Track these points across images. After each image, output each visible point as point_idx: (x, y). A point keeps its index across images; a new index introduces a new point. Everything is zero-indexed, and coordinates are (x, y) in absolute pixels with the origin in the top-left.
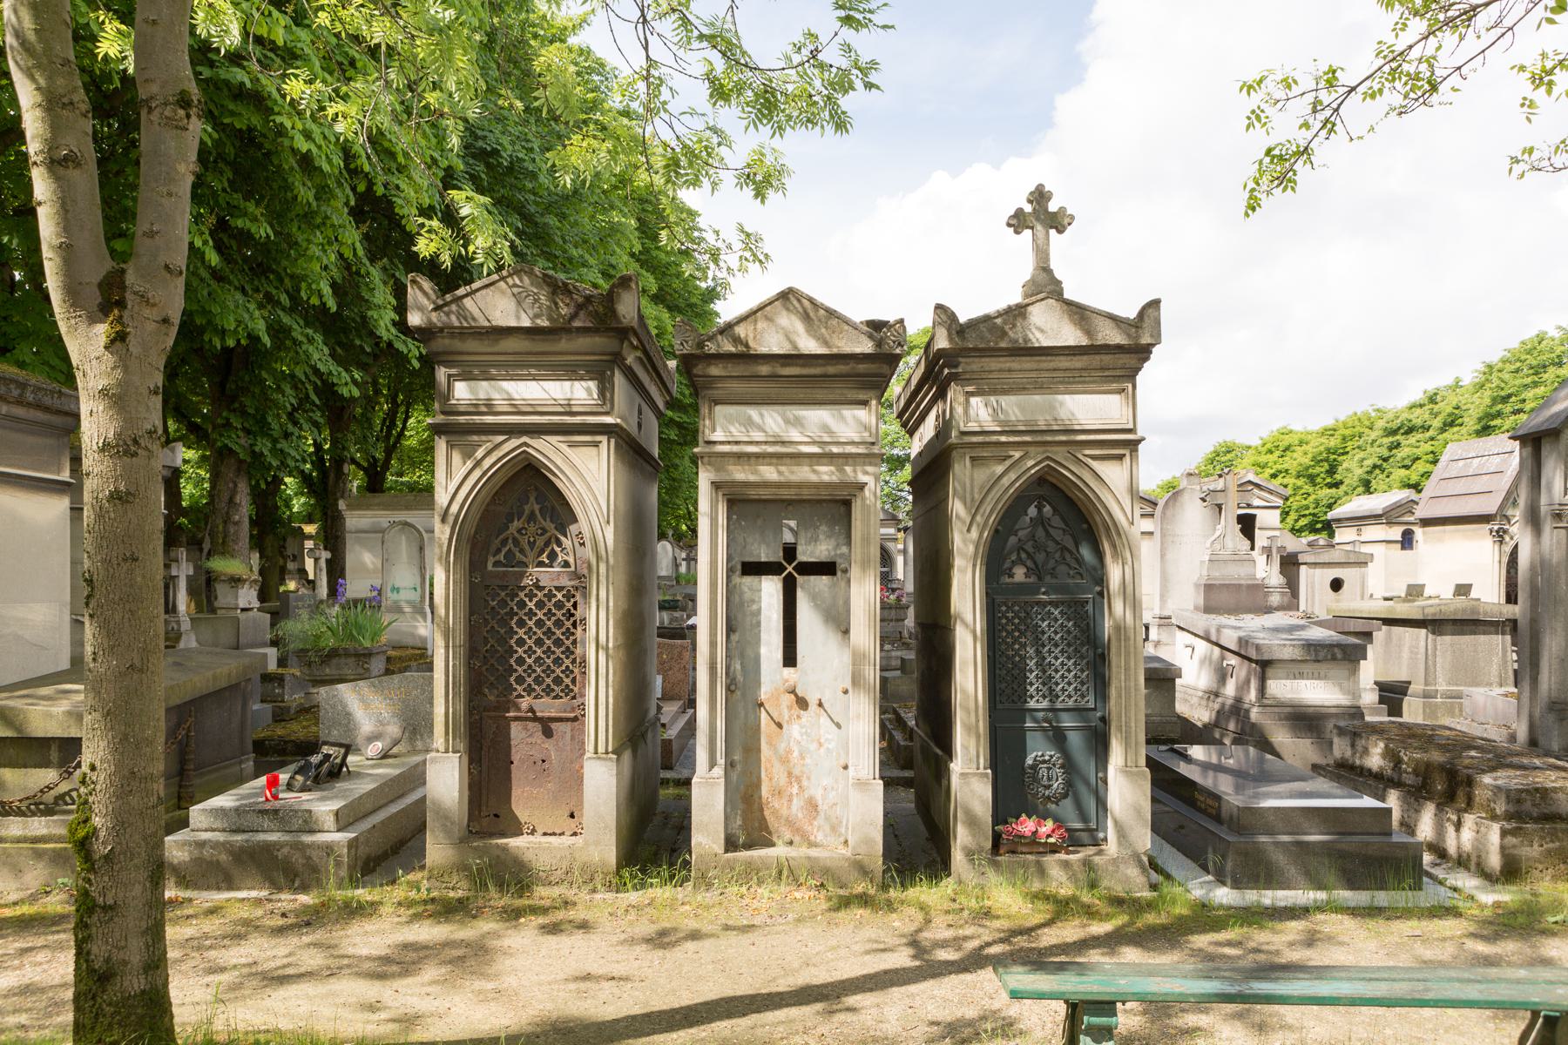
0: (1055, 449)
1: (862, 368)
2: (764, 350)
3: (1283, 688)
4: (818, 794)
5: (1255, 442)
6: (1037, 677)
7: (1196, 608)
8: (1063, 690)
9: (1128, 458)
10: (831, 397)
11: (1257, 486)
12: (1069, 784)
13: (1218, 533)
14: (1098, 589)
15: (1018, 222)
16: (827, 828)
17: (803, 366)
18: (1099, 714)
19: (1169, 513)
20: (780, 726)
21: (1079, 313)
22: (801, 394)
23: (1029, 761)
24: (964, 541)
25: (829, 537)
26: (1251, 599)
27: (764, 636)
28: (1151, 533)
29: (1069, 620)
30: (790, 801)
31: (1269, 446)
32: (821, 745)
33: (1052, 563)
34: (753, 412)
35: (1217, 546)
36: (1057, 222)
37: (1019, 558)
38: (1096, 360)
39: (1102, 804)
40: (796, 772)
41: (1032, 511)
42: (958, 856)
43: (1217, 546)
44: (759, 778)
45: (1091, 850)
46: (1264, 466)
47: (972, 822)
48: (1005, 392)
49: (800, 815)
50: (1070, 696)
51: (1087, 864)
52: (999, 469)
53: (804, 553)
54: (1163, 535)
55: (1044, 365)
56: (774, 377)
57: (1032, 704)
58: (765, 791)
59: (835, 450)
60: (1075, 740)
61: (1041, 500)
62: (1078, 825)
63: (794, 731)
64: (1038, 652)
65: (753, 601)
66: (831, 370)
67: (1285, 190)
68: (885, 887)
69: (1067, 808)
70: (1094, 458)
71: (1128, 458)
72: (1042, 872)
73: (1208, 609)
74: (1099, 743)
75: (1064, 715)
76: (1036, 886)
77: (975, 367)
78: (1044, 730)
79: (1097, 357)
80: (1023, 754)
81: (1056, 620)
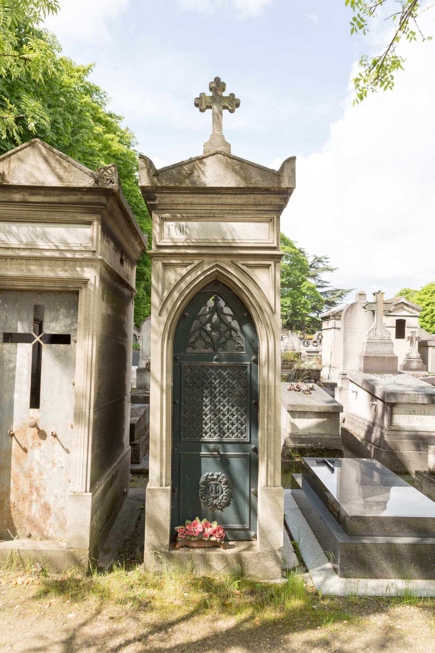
0: (222, 259)
1: (87, 198)
2: (14, 182)
3: (403, 420)
4: (51, 500)
5: (419, 289)
6: (211, 419)
7: (360, 370)
8: (228, 429)
9: (272, 267)
10: (65, 218)
11: (406, 305)
12: (231, 496)
13: (373, 327)
14: (254, 357)
15: (201, 104)
16: (56, 525)
17: (45, 195)
18: (253, 446)
19: (349, 315)
20: (25, 450)
21: (241, 166)
22: (44, 215)
23: (202, 480)
24: (159, 323)
25: (66, 317)
26: (388, 365)
27: (17, 386)
28: (339, 329)
29: (233, 379)
30: (31, 505)
31: (425, 291)
32: (54, 465)
33: (223, 340)
34: (14, 227)
35: (372, 334)
36: (233, 103)
37: (201, 336)
38: (252, 198)
39: (253, 510)
40: (37, 483)
41: (211, 303)
42: (147, 552)
43: (372, 334)
44: (9, 488)
45: (243, 546)
46: (422, 301)
47: (156, 526)
48: (188, 219)
49: (37, 516)
50: (233, 433)
51: (239, 558)
52: (184, 271)
53: (48, 328)
54: (345, 328)
55: (216, 201)
56: (24, 202)
57: (206, 438)
58: (13, 497)
59: (69, 255)
60: (236, 465)
61: (219, 295)
62: (237, 526)
63: (36, 454)
64: (211, 401)
65: (10, 361)
66: (65, 199)
67: (385, 88)
68: (89, 574)
69: (229, 513)
70: (249, 266)
71: (272, 267)
72: (206, 561)
73: (366, 371)
74: (252, 465)
75: (229, 447)
76: (201, 572)
77: (167, 201)
78: (214, 457)
79: (252, 196)
80: (199, 475)
81: (225, 379)
